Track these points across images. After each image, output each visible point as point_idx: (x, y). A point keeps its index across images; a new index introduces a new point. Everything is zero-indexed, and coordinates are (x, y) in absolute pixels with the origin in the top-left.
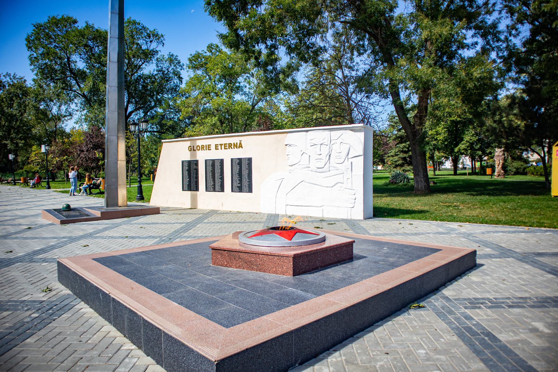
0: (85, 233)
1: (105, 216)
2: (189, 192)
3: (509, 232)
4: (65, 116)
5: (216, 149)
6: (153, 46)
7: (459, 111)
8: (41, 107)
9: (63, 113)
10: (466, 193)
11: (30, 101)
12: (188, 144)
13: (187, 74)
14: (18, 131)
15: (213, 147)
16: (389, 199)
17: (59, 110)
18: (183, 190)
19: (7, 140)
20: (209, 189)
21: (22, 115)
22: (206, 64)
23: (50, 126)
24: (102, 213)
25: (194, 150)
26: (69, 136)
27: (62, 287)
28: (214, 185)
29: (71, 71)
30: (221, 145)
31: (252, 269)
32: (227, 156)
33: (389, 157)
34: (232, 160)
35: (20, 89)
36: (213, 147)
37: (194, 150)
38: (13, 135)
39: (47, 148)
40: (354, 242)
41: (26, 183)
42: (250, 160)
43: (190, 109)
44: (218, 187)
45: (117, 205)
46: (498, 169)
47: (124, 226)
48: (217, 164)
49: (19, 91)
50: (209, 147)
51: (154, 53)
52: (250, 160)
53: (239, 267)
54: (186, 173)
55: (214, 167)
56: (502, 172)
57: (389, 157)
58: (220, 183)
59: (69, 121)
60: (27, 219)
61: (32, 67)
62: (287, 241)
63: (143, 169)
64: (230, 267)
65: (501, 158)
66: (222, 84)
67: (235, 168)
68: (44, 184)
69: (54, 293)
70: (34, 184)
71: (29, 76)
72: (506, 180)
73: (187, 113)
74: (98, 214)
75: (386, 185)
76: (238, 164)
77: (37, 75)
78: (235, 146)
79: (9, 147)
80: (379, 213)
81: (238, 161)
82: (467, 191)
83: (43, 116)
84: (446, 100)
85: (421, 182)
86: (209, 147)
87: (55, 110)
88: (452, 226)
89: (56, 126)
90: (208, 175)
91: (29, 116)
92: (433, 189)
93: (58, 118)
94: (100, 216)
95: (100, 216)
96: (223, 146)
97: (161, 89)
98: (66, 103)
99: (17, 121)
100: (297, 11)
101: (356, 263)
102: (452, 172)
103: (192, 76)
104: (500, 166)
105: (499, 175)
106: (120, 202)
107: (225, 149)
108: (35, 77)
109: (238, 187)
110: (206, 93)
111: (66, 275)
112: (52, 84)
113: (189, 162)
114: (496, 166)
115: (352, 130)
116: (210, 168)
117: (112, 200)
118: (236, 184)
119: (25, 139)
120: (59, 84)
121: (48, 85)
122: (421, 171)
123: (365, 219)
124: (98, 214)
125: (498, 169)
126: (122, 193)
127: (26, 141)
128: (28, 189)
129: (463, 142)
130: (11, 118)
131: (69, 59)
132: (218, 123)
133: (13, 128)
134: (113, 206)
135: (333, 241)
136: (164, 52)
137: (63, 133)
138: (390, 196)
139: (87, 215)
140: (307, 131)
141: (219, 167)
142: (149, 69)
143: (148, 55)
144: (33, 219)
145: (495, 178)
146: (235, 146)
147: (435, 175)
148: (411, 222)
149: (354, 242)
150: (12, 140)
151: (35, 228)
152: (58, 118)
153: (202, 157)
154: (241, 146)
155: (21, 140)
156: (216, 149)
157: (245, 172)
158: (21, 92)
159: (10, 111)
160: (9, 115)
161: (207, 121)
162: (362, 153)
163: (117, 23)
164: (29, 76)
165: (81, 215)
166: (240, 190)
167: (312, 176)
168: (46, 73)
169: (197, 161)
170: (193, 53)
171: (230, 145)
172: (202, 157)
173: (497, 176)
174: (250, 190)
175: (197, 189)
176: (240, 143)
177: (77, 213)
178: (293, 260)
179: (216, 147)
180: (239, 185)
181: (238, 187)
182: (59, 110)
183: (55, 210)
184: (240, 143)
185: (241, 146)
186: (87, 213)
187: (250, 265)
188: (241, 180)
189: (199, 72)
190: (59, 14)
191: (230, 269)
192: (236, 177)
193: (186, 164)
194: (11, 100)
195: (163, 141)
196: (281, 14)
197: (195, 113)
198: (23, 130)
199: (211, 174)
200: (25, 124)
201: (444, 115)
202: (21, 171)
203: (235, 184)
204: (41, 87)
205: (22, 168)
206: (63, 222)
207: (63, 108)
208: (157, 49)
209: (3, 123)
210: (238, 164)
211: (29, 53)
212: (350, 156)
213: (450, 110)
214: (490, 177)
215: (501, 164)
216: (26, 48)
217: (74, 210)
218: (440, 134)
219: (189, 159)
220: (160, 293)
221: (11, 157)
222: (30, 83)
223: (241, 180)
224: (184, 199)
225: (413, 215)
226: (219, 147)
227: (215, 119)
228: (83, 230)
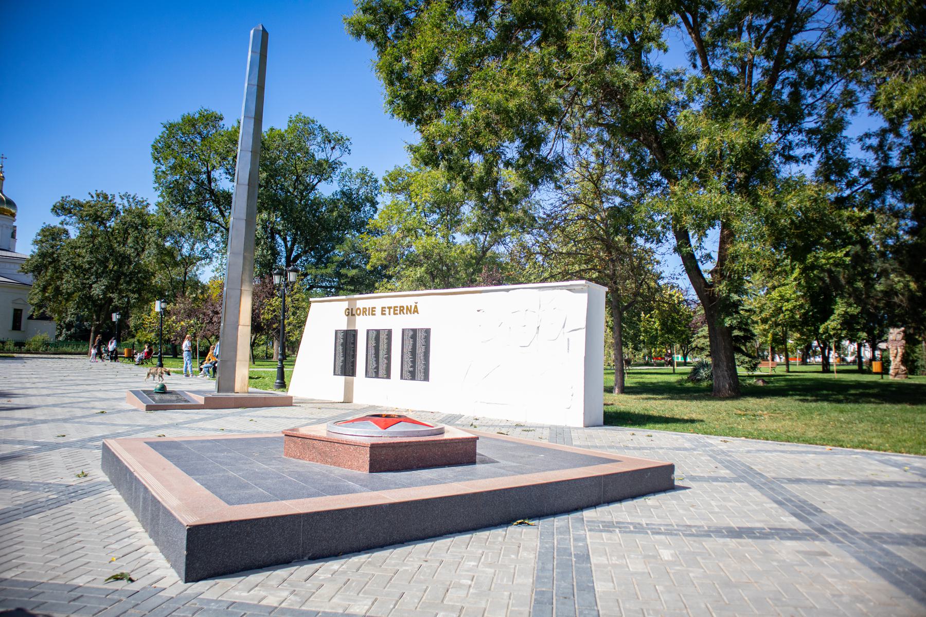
0: (171, 422)
1: (212, 403)
2: (343, 377)
3: (792, 452)
4: (201, 259)
5: (383, 314)
6: (335, 155)
7: (767, 263)
8: (168, 244)
9: (197, 253)
10: (797, 397)
11: (151, 236)
12: (345, 305)
13: (385, 200)
14: (131, 279)
15: (378, 311)
16: (670, 403)
17: (192, 249)
18: (335, 374)
19: (113, 293)
20: (370, 375)
21: (138, 255)
22: (409, 184)
23: (176, 273)
24: (206, 399)
25: (353, 315)
26: (204, 289)
27: (103, 474)
28: (377, 368)
29: (212, 192)
30: (390, 308)
31: (327, 462)
32: (397, 325)
33: (699, 337)
34: (403, 330)
35: (139, 217)
36: (378, 311)
37: (353, 315)
38: (123, 287)
39: (163, 305)
40: (478, 438)
41: (131, 357)
42: (428, 332)
43: (384, 255)
44: (382, 371)
45: (233, 390)
46: (895, 363)
47: (230, 418)
48: (383, 337)
49: (137, 221)
50: (372, 311)
51: (333, 166)
52: (428, 332)
53: (312, 460)
54: (340, 348)
55: (380, 339)
56: (903, 368)
57: (699, 337)
58: (385, 366)
59: (207, 267)
60: (107, 402)
61: (157, 185)
62: (380, 429)
63: (278, 336)
64: (303, 459)
65: (900, 344)
66: (436, 216)
67: (406, 342)
68: (156, 361)
69: (87, 479)
70: (141, 359)
71: (152, 199)
72: (912, 382)
73: (378, 260)
74: (201, 400)
75: (680, 382)
76: (412, 338)
77: (162, 196)
78: (409, 310)
79: (116, 302)
80: (613, 419)
81: (411, 333)
82: (800, 395)
83: (168, 257)
84: (746, 245)
85: (724, 377)
86: (372, 311)
87: (186, 251)
88: (710, 441)
89: (186, 273)
90: (370, 354)
91: (148, 258)
92: (740, 390)
93: (189, 261)
94: (203, 403)
95: (203, 403)
96: (392, 310)
97: (345, 224)
98: (200, 240)
99: (130, 263)
100: (512, 111)
101: (478, 467)
102: (820, 368)
103: (388, 203)
104: (899, 359)
105: (897, 374)
106: (238, 386)
107: (395, 314)
108: (160, 200)
109: (410, 372)
110: (409, 230)
111: (111, 461)
112: (183, 212)
113: (346, 333)
114: (891, 359)
115: (570, 289)
116: (373, 343)
117: (226, 384)
118: (407, 367)
119: (139, 292)
120: (194, 212)
121: (178, 212)
122: (723, 358)
123: (587, 426)
124: (201, 400)
125: (895, 363)
126: (242, 370)
127: (140, 295)
128: (132, 366)
129: (832, 318)
130: (123, 259)
131: (208, 173)
132: (428, 277)
133: (123, 274)
134: (227, 391)
135: (453, 433)
136: (352, 162)
137: (196, 285)
138: (671, 399)
139: (186, 401)
140: (508, 290)
141: (386, 341)
142: (326, 190)
143: (324, 169)
144: (114, 403)
145: (890, 378)
146: (409, 310)
147: (788, 371)
148: (649, 433)
149: (478, 438)
150: (121, 292)
151: (110, 413)
152: (189, 261)
153: (363, 325)
154: (416, 311)
155: (134, 293)
156: (383, 314)
157: (420, 350)
158: (140, 222)
159: (120, 249)
160: (121, 255)
161: (408, 273)
162: (583, 324)
163: (251, 131)
164: (152, 199)
165: (178, 400)
166: (413, 376)
167: (515, 359)
168: (177, 194)
169: (355, 331)
170: (391, 169)
171: (402, 309)
172: (363, 325)
173: (896, 374)
174: (426, 378)
175: (353, 373)
176: (416, 307)
177: (174, 398)
178: (371, 451)
179: (382, 311)
180: (411, 369)
181: (410, 372)
182: (192, 249)
183: (144, 391)
184: (416, 307)
185: (416, 311)
186: (187, 398)
187: (324, 457)
188: (414, 362)
189: (402, 197)
190: (193, 109)
191: (301, 461)
192: (408, 358)
193: (340, 335)
194: (126, 231)
195: (311, 299)
196: (487, 117)
197: (393, 260)
198: (138, 278)
199: (373, 352)
200: (139, 269)
201: (743, 269)
202: (132, 340)
203: (405, 367)
204: (167, 214)
205: (134, 336)
206: (150, 408)
207: (199, 246)
208: (341, 160)
209: (111, 266)
210: (412, 338)
211: (154, 166)
212: (567, 329)
213: (753, 261)
214: (879, 376)
215: (900, 354)
216: (151, 160)
217: (171, 393)
218: (788, 300)
219: (344, 327)
220: (190, 472)
221: (115, 317)
222: (152, 209)
223: (414, 362)
224: (333, 387)
225: (673, 426)
226: (387, 310)
227: (420, 271)
228: (171, 419)
